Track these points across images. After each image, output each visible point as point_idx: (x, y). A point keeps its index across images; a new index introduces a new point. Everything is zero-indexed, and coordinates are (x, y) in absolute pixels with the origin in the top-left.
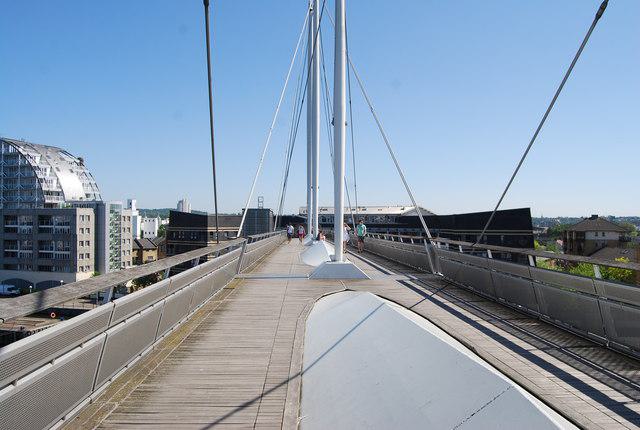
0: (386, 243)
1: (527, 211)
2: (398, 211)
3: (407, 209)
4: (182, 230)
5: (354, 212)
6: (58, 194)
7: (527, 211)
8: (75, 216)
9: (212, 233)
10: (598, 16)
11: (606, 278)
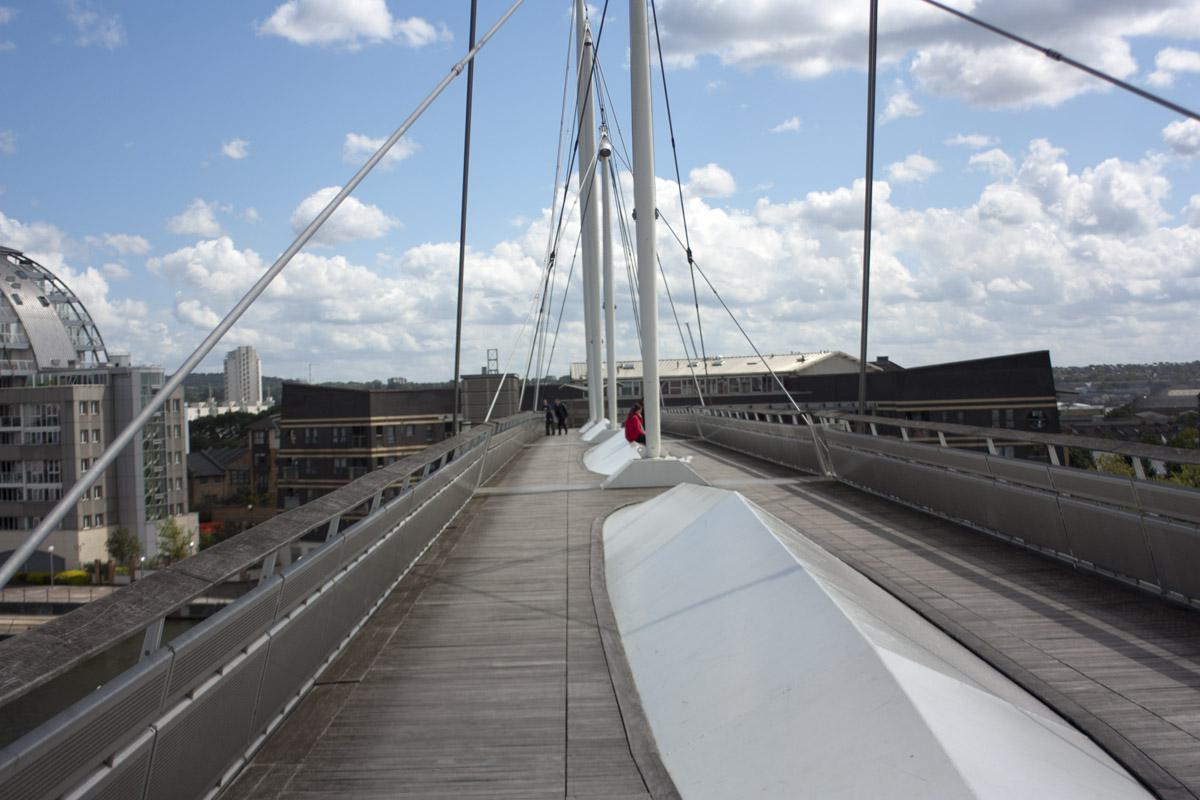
0: (732, 422)
1: (1044, 356)
2: (791, 365)
3: (810, 359)
4: (313, 424)
5: (699, 370)
6: (21, 353)
7: (1044, 356)
8: (70, 403)
9: (380, 429)
10: (674, 146)
11: (934, 434)
